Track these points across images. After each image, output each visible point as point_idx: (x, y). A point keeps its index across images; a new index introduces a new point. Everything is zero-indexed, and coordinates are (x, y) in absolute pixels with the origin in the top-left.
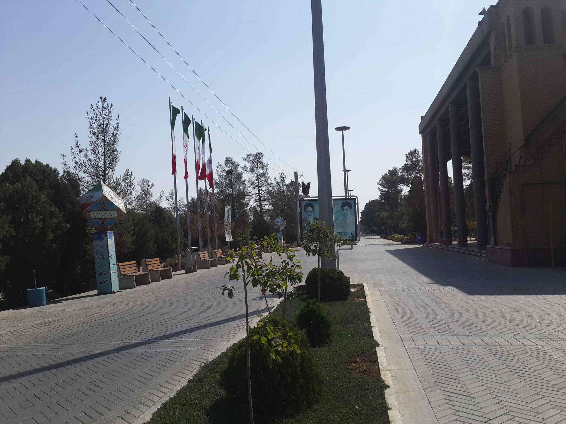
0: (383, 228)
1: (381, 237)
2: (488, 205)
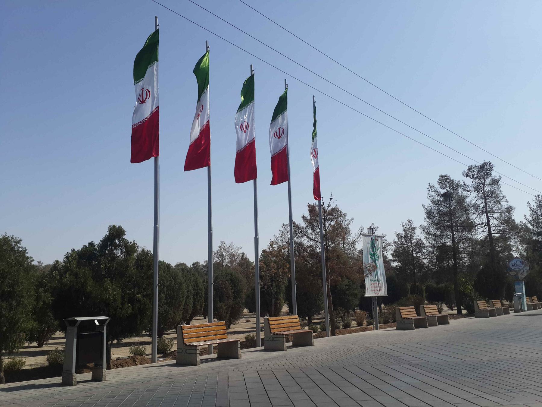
2: (525, 304)
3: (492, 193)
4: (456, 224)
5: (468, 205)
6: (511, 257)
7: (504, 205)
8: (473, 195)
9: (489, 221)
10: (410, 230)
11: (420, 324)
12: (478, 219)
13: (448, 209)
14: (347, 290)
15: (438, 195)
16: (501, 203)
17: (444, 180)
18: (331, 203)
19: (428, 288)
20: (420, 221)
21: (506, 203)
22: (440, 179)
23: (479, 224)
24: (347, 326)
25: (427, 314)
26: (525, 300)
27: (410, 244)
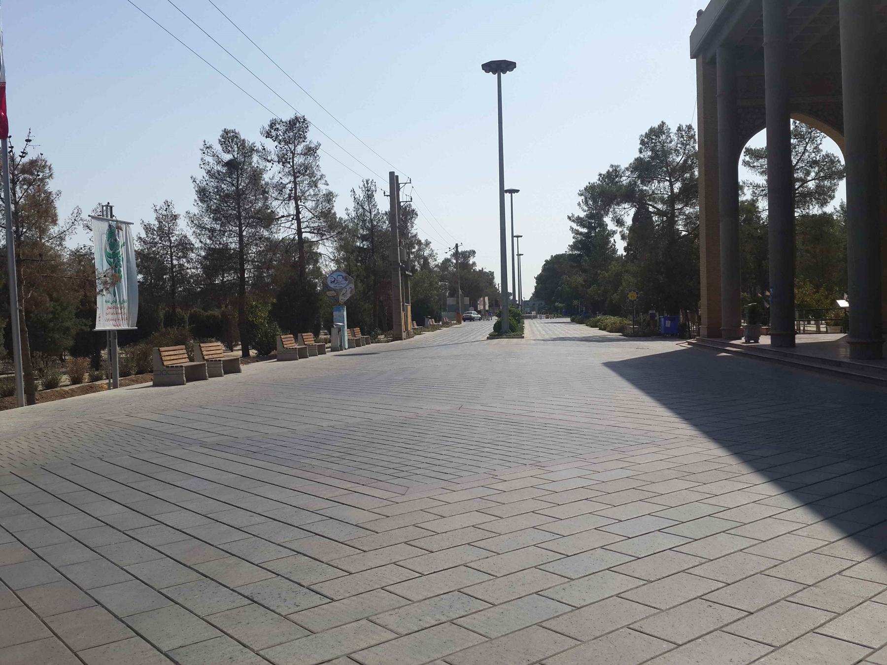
0: (575, 302)
1: (573, 321)
2: (346, 338)
3: (306, 168)
4: (248, 213)
5: (267, 184)
6: (317, 272)
7: (323, 188)
8: (278, 167)
9: (298, 213)
10: (168, 219)
11: (195, 374)
12: (282, 208)
13: (234, 186)
14: (50, 321)
15: (218, 163)
16: (319, 185)
17: (229, 138)
18: (27, 150)
19: (193, 318)
20: (187, 204)
21: (326, 187)
22: (222, 136)
23: (283, 216)
24: (52, 384)
25: (206, 357)
26: (346, 334)
27: (167, 243)
